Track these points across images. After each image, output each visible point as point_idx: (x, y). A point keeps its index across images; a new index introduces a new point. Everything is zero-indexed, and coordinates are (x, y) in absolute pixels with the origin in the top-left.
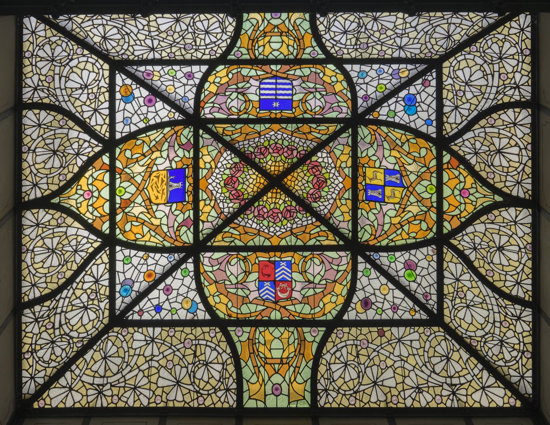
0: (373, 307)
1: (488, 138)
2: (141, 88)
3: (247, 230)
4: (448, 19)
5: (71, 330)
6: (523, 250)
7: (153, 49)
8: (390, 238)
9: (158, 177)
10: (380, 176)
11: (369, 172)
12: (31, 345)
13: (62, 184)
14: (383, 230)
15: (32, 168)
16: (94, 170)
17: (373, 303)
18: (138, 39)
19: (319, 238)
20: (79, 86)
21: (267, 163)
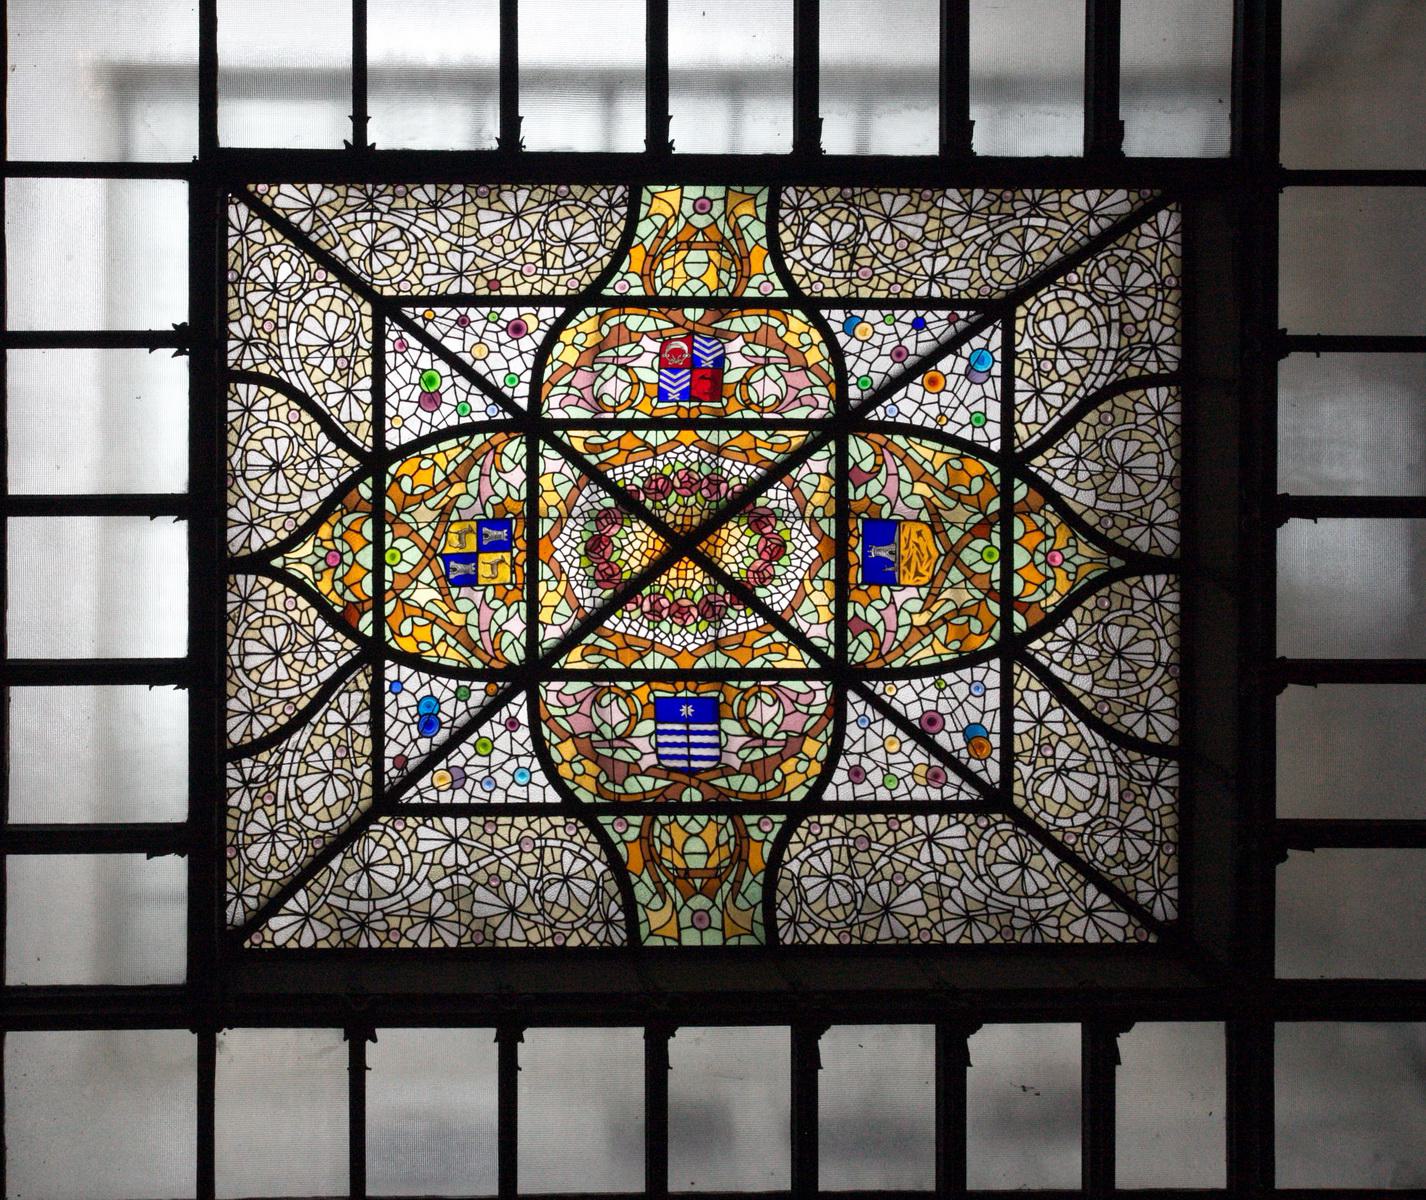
0: (504, 325)
1: (295, 676)
2: (950, 749)
3: (742, 457)
4: (375, 910)
5: (1087, 310)
6: (238, 473)
7: (930, 838)
8: (468, 452)
9: (917, 573)
10: (484, 571)
11: (504, 574)
12: (1164, 301)
13: (1104, 591)
14: (481, 466)
15: (1160, 634)
16: (1043, 604)
17: (505, 330)
18: (959, 864)
19: (603, 440)
20: (1072, 775)
21: (702, 585)
